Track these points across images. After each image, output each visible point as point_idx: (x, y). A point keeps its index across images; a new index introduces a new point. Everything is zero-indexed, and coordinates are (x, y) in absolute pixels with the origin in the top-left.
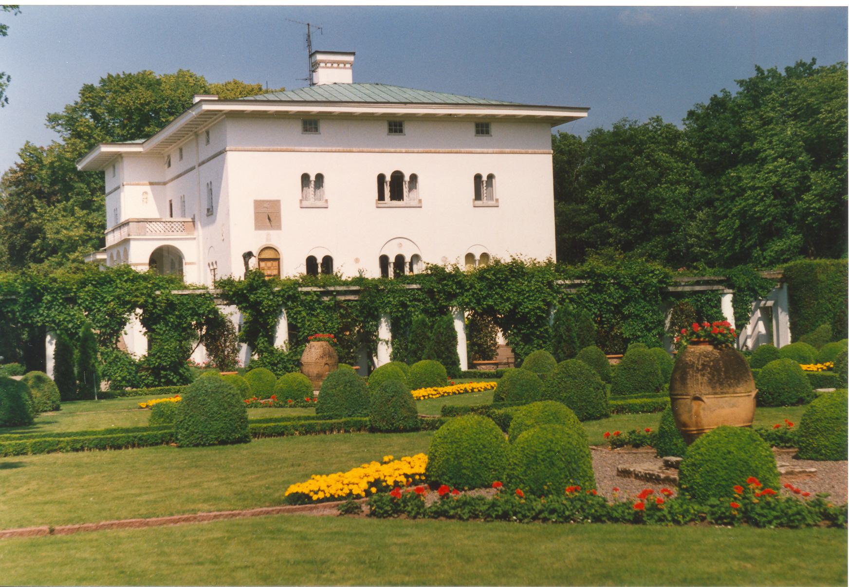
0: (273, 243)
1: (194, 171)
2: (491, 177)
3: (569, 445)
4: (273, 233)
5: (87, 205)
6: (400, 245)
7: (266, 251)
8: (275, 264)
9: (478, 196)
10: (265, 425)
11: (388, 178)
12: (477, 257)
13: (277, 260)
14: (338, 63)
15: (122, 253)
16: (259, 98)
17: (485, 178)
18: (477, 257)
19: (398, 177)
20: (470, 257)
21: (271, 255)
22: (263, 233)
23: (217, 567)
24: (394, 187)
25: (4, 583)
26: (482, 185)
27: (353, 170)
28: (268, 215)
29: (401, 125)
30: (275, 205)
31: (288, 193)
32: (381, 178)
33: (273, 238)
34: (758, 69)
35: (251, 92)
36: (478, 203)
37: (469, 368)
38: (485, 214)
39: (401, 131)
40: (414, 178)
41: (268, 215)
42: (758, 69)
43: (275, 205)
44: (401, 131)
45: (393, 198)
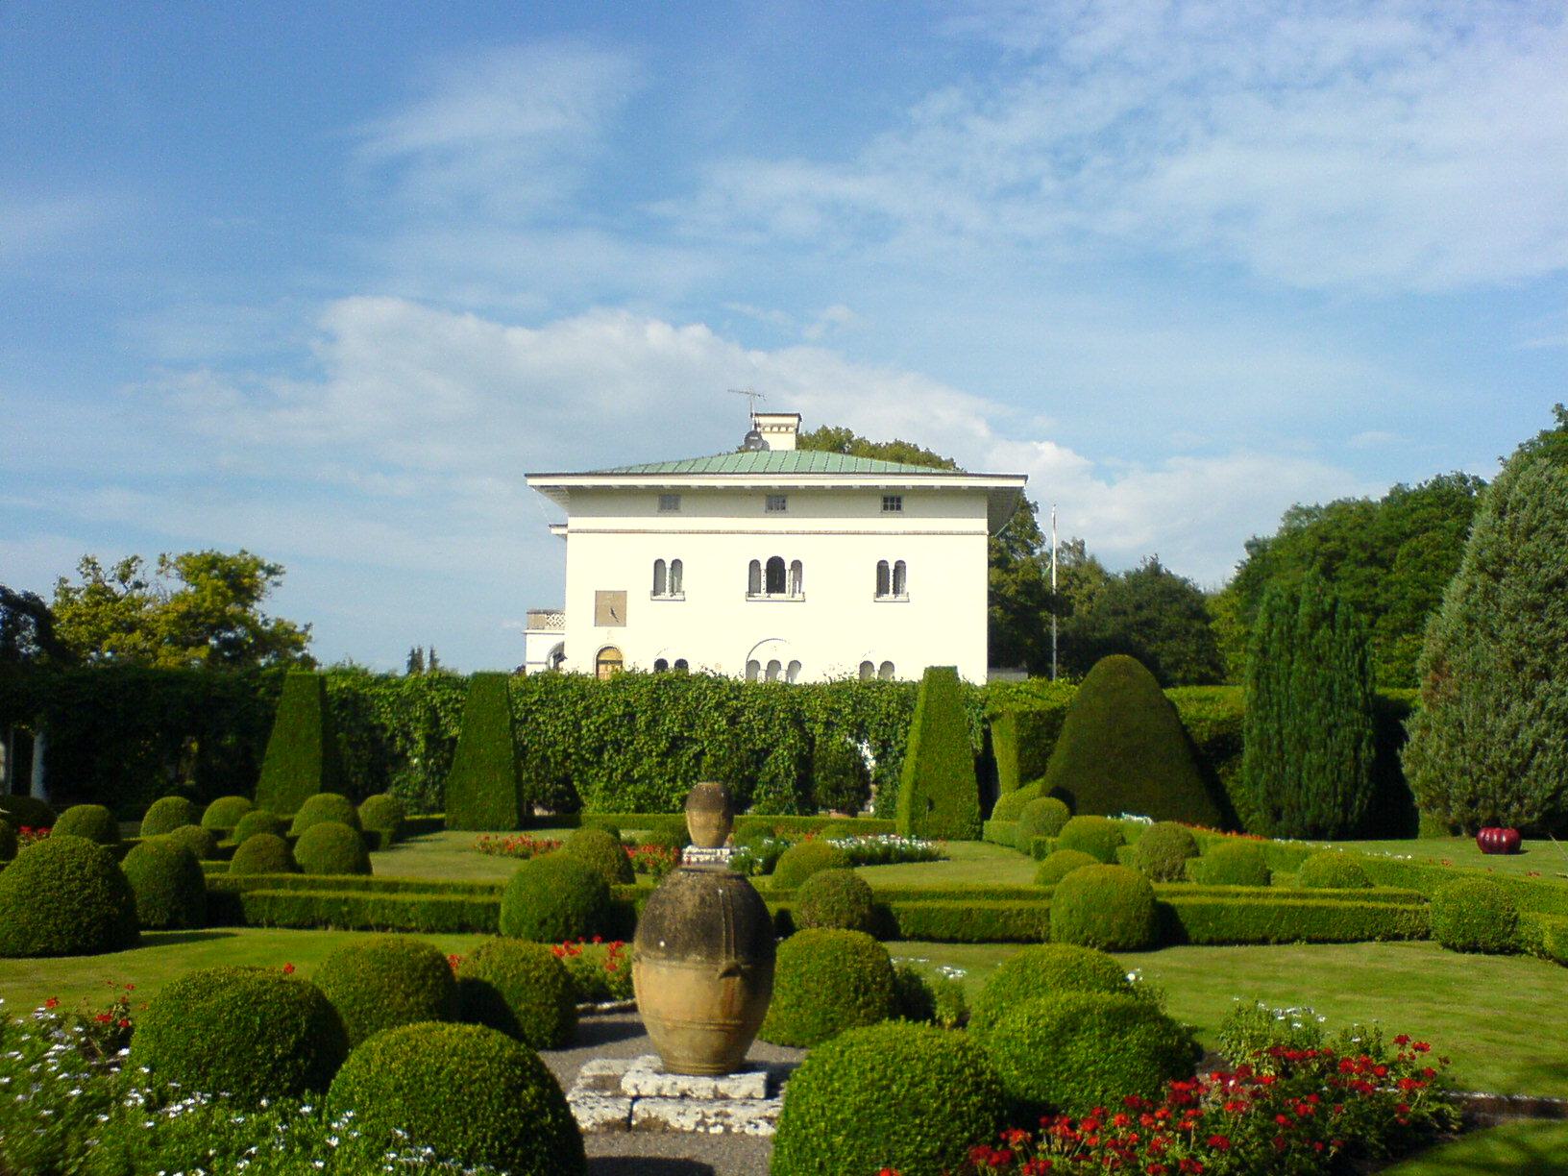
2: (677, 564)
3: (819, 729)
4: (616, 630)
9: (882, 589)
11: (763, 566)
12: (671, 665)
18: (671, 665)
19: (776, 566)
20: (661, 664)
22: (604, 630)
24: (775, 576)
26: (889, 579)
27: (719, 549)
28: (611, 609)
29: (899, 500)
30: (621, 596)
32: (754, 565)
37: (1001, 654)
39: (899, 508)
40: (797, 565)
41: (611, 609)
43: (621, 596)
44: (899, 508)
45: (770, 589)
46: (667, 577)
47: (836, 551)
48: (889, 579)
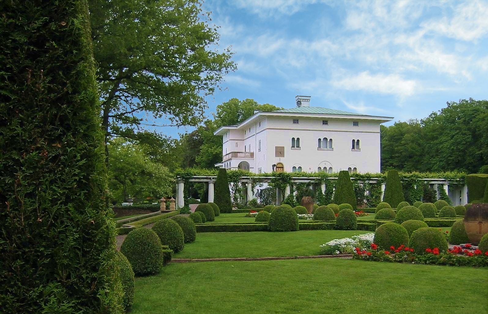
0: (281, 162)
1: (254, 136)
5: (392, 151)
6: (325, 164)
7: (280, 164)
8: (282, 169)
10: (303, 223)
13: (283, 168)
14: (305, 100)
15: (226, 164)
16: (278, 111)
17: (356, 141)
21: (280, 166)
23: (450, 291)
25: (482, 307)
26: (355, 144)
27: (309, 136)
28: (280, 152)
30: (283, 148)
33: (282, 160)
34: (448, 103)
35: (278, 109)
36: (353, 150)
38: (356, 153)
40: (331, 140)
42: (448, 103)
43: (283, 148)
46: (296, 143)
47: (341, 138)
48: (355, 144)
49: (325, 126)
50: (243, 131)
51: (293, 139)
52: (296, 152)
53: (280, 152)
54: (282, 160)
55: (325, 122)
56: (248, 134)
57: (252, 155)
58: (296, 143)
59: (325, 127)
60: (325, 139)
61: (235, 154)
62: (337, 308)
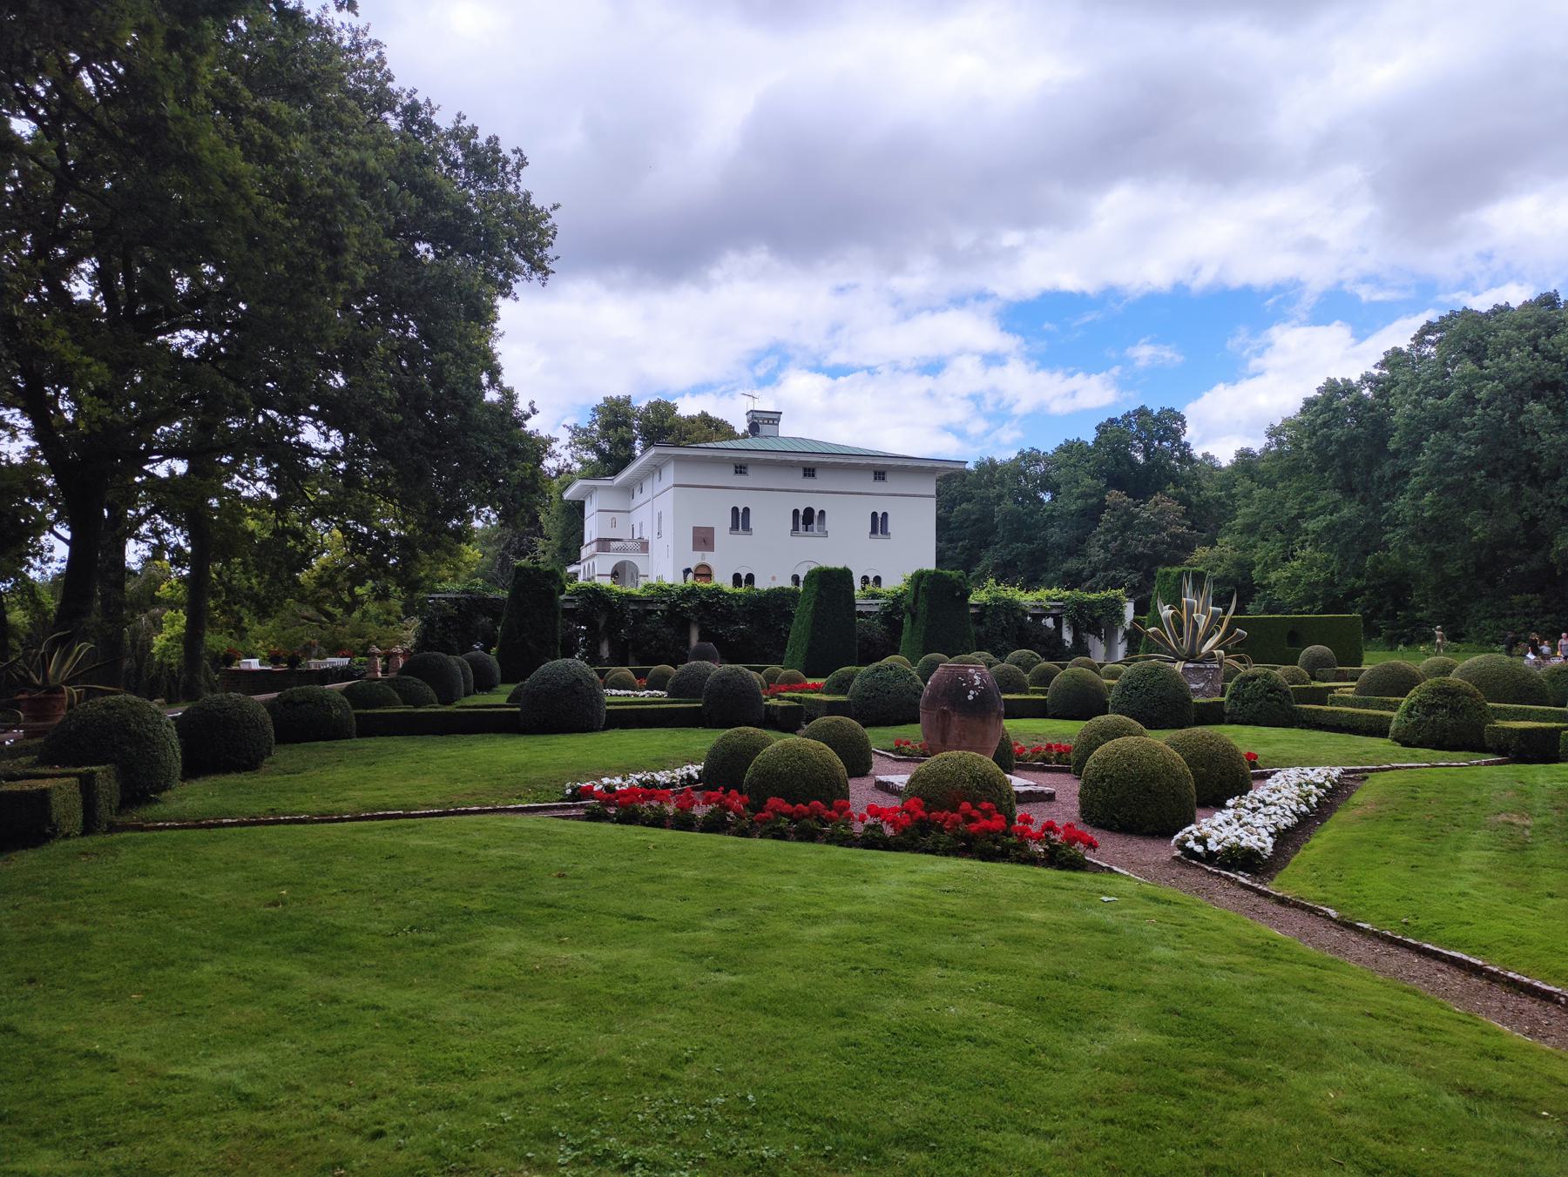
21: (704, 572)
26: (879, 525)
31: (721, 523)
32: (796, 512)
33: (709, 558)
38: (879, 542)
40: (822, 513)
42: (461, 117)
46: (741, 520)
48: (879, 525)
49: (739, 477)
50: (629, 490)
51: (735, 510)
52: (740, 539)
53: (703, 539)
54: (709, 558)
55: (809, 472)
56: (639, 498)
57: (644, 546)
58: (741, 520)
59: (809, 483)
60: (809, 511)
61: (604, 544)
62: (501, 1148)
